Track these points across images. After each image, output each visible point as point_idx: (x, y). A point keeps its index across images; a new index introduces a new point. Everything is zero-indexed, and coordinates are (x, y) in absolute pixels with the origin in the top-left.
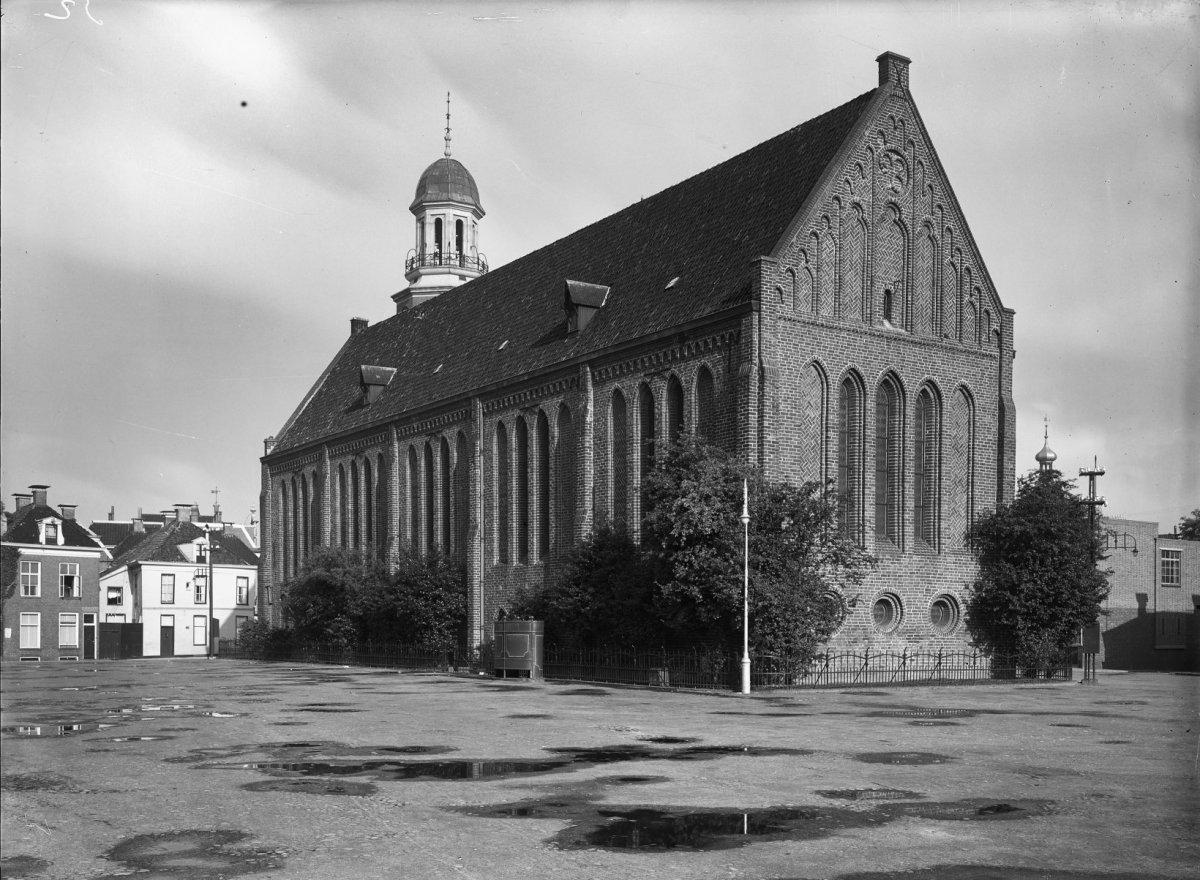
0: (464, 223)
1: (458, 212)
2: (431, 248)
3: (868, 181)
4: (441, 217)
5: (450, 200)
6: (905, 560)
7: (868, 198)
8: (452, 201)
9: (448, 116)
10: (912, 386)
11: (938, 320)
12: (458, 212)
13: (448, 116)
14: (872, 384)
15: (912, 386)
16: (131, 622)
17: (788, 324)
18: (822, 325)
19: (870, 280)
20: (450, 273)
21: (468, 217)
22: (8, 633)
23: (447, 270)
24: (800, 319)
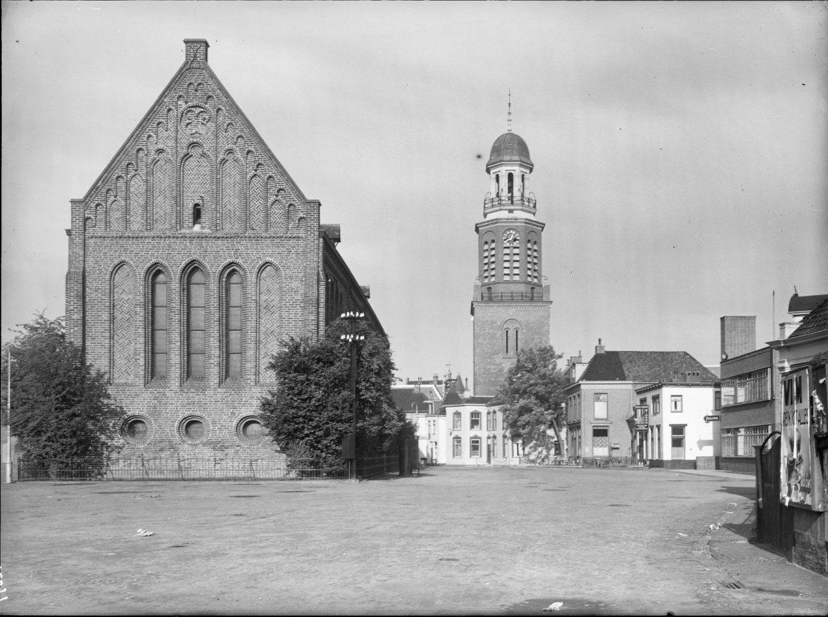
0: (514, 175)
1: (509, 168)
2: (505, 194)
3: (171, 133)
4: (512, 172)
5: (501, 161)
6: (209, 393)
7: (171, 143)
8: (504, 161)
9: (509, 104)
10: (213, 266)
11: (246, 218)
12: (509, 168)
13: (509, 104)
14: (175, 271)
15: (213, 266)
16: (754, 478)
17: (98, 241)
18: (129, 237)
19: (178, 201)
20: (501, 210)
21: (517, 171)
22: (556, 606)
23: (498, 208)
24: (109, 235)
